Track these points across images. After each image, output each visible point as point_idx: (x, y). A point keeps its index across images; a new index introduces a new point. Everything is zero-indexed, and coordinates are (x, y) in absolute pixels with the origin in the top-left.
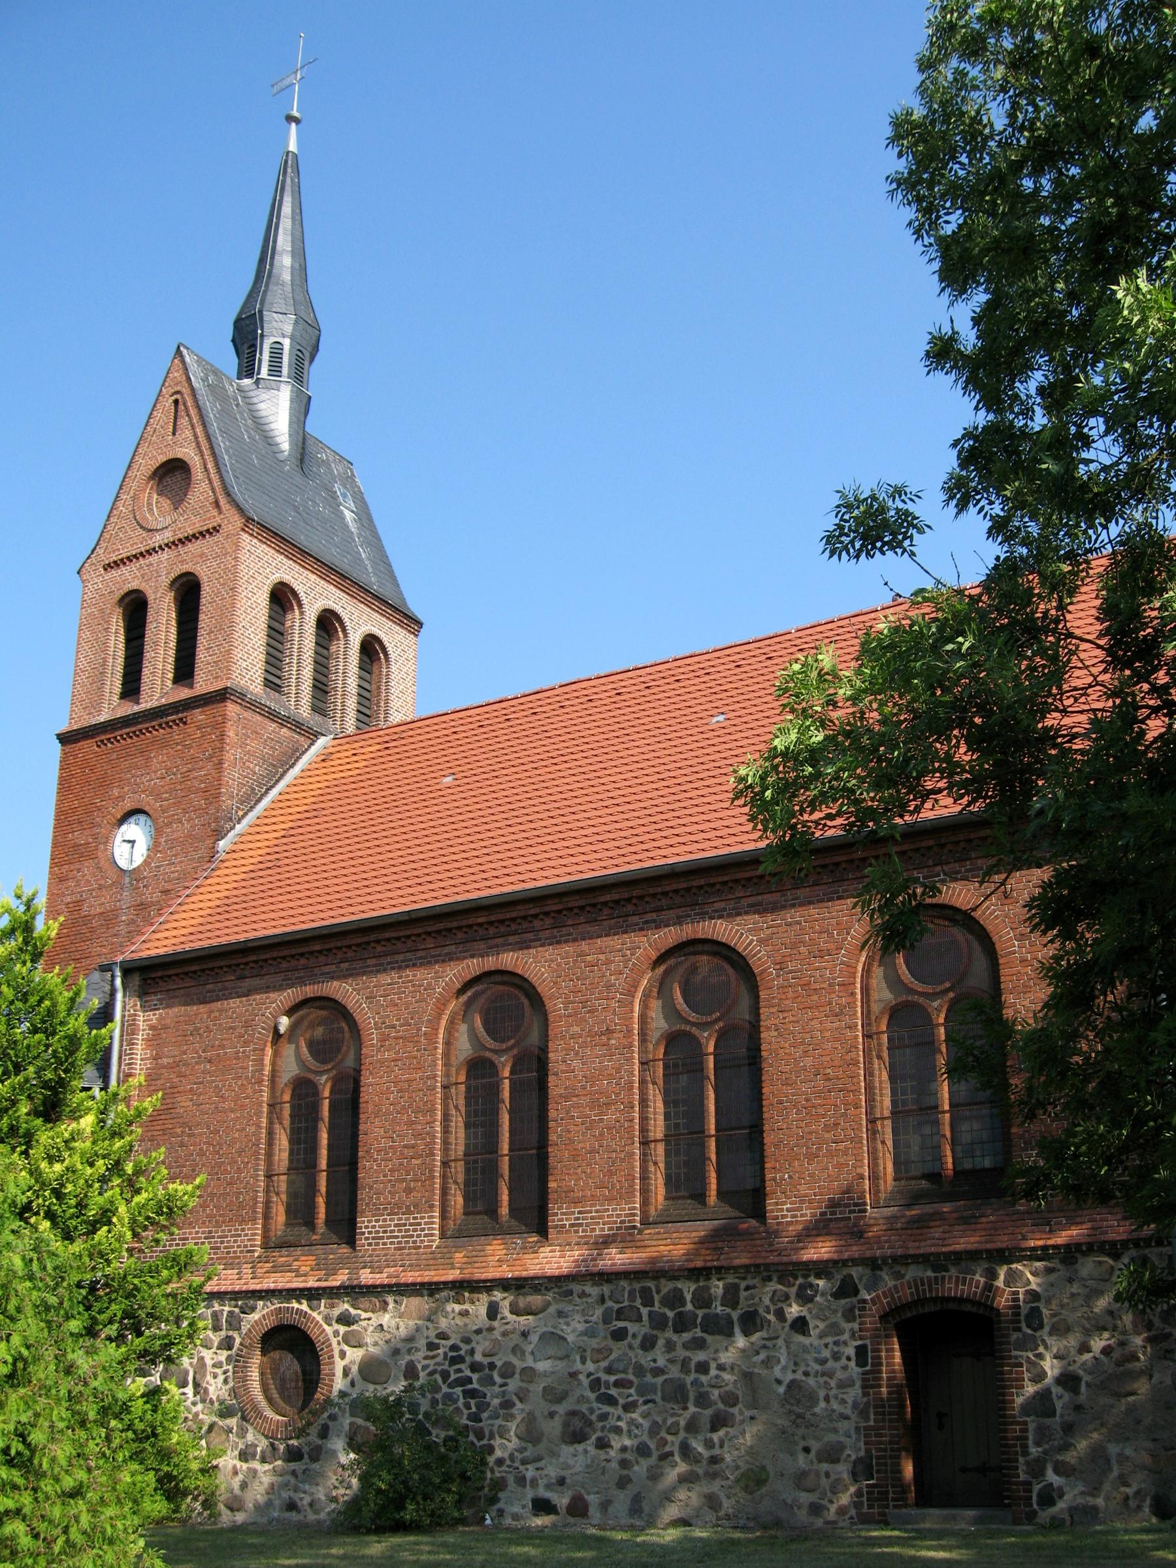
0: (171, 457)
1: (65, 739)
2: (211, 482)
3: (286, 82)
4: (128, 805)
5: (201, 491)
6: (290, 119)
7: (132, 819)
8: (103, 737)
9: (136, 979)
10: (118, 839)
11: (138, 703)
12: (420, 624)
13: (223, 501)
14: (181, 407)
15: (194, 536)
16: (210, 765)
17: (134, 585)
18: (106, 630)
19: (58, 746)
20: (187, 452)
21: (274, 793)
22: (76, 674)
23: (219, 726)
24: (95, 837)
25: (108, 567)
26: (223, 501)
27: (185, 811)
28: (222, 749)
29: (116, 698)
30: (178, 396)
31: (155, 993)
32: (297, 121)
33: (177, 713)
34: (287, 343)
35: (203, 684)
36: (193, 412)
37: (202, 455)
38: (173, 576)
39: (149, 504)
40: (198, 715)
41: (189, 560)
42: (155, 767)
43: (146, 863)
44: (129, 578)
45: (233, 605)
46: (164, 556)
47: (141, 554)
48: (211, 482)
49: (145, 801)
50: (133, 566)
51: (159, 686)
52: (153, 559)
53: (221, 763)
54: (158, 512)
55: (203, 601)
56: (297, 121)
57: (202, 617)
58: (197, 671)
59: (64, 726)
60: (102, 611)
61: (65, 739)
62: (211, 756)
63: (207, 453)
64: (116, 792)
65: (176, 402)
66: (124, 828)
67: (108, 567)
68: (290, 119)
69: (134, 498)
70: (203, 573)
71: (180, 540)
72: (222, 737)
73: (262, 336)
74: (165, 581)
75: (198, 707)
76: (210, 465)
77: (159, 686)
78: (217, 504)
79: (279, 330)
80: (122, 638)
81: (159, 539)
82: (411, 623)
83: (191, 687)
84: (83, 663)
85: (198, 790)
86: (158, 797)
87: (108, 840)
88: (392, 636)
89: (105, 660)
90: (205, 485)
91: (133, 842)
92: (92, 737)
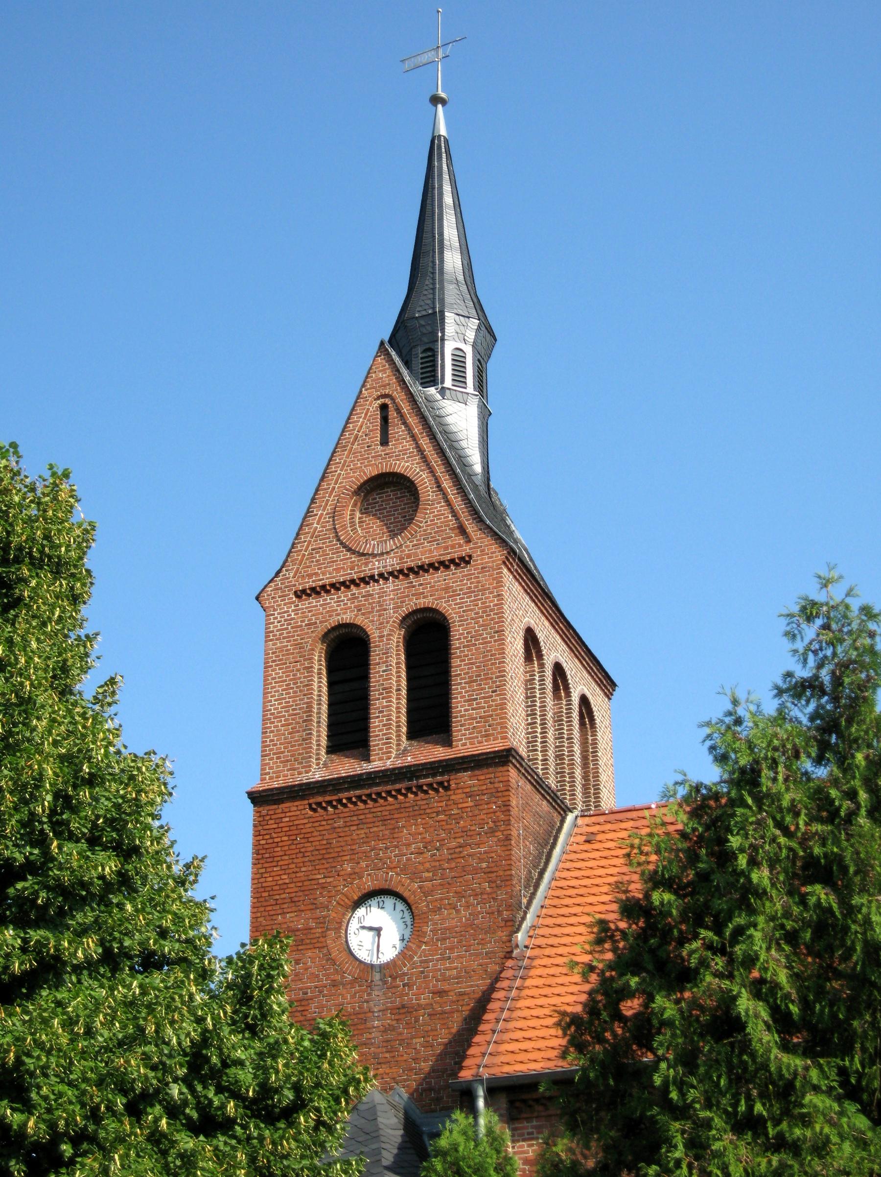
0: (385, 469)
1: (257, 798)
2: (449, 503)
3: (425, 58)
4: (369, 884)
5: (435, 513)
6: (436, 100)
7: (374, 902)
8: (320, 799)
9: (503, 1101)
10: (354, 925)
11: (367, 758)
12: (613, 684)
13: (471, 527)
14: (392, 414)
15: (431, 565)
16: (492, 841)
17: (347, 617)
18: (309, 669)
19: (249, 807)
20: (408, 465)
21: (547, 876)
22: (265, 720)
23: (503, 792)
24: (321, 922)
25: (300, 594)
26: (471, 527)
27: (460, 895)
28: (508, 823)
29: (323, 751)
30: (387, 401)
31: (528, 1119)
32: (443, 102)
33: (434, 775)
34: (468, 350)
35: (466, 741)
36: (412, 420)
37: (432, 472)
38: (404, 611)
39: (353, 524)
40: (466, 779)
41: (428, 593)
42: (410, 838)
43: (403, 955)
44: (340, 609)
45: (502, 651)
46: (391, 585)
47: (353, 581)
48: (449, 503)
49: (394, 879)
50: (343, 595)
51: (391, 742)
52: (373, 588)
53: (508, 838)
54: (369, 532)
55: (455, 644)
56: (443, 102)
57: (455, 662)
58: (455, 727)
59: (255, 783)
60: (299, 646)
61: (257, 798)
62: (492, 832)
63: (440, 470)
64: (348, 868)
65: (384, 408)
66: (361, 911)
67: (300, 594)
68: (436, 100)
69: (333, 515)
70: (450, 609)
71: (411, 569)
72: (506, 807)
73: (443, 339)
74: (394, 615)
75: (465, 770)
76: (447, 484)
77: (391, 742)
78: (462, 530)
79: (457, 336)
80: (325, 680)
81: (376, 566)
82: (607, 684)
83: (448, 743)
84: (275, 706)
85: (476, 871)
86: (415, 876)
87: (340, 927)
88: (597, 700)
89: (310, 707)
90: (440, 507)
91: (378, 931)
92: (303, 798)
